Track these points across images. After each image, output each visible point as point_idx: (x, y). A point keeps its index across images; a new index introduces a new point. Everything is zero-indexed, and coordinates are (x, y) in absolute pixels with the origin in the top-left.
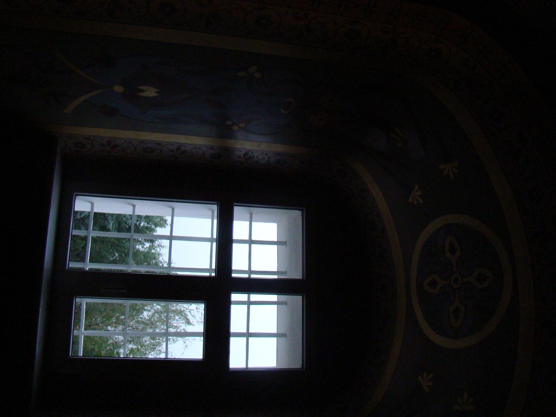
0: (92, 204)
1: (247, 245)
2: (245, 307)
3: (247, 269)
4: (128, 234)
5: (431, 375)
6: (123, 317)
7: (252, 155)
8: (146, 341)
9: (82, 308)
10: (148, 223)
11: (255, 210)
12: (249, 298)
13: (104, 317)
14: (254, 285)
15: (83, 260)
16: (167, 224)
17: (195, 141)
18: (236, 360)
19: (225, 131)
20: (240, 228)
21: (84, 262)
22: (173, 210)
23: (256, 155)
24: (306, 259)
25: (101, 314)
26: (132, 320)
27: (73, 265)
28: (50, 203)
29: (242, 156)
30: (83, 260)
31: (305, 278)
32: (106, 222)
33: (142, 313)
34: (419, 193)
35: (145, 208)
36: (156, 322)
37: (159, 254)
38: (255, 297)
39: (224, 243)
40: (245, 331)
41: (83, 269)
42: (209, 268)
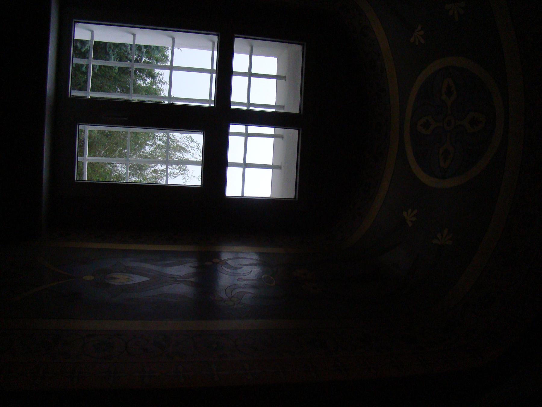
0: (92, 32)
1: (246, 78)
2: (243, 138)
3: (245, 101)
5: (415, 212)
6: (126, 151)
8: (148, 174)
9: (85, 141)
10: (149, 59)
11: (255, 43)
12: (247, 129)
13: (108, 150)
14: (251, 117)
15: (84, 88)
16: (168, 60)
18: (233, 188)
20: (240, 62)
21: (86, 90)
22: (173, 39)
24: (304, 97)
25: (105, 148)
26: (134, 154)
27: (75, 93)
28: (50, 30)
30: (84, 88)
31: (302, 112)
33: (144, 148)
35: (146, 37)
36: (158, 156)
37: (161, 90)
38: (252, 129)
39: (224, 74)
40: (241, 161)
41: (85, 97)
42: (208, 99)
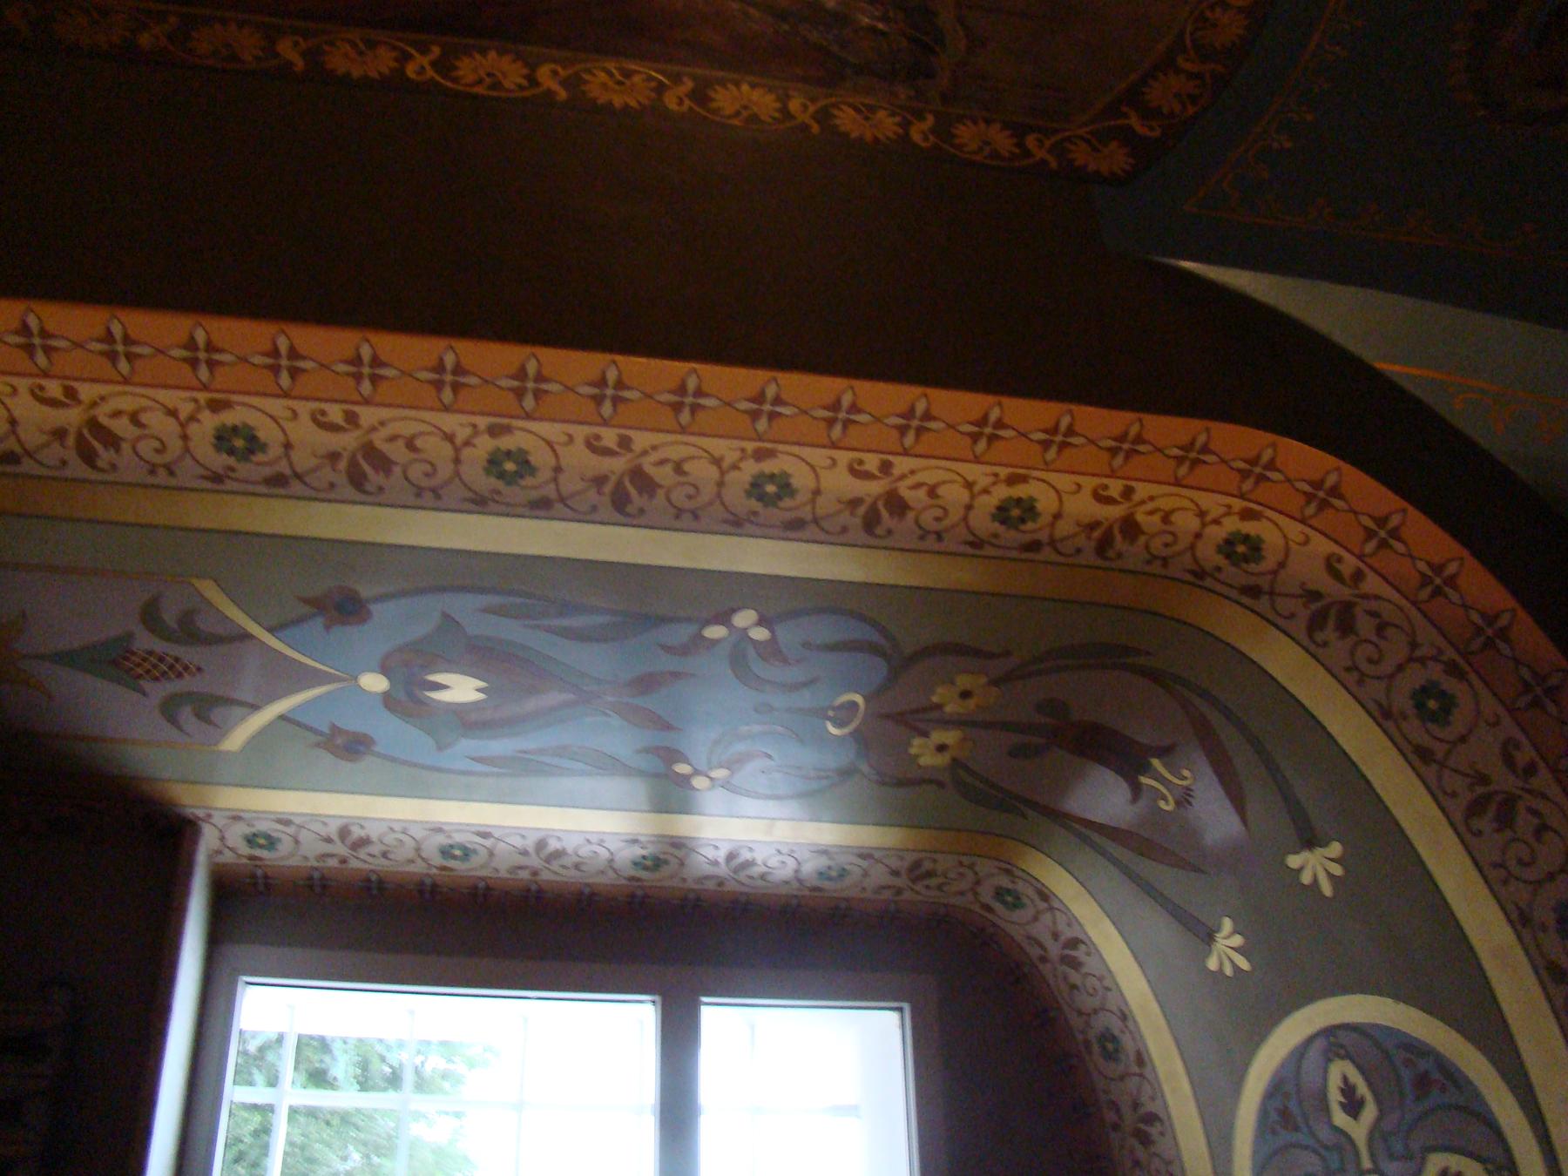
4: (391, 1094)
7: (362, 833)
17: (580, 822)
19: (670, 789)
23: (759, 856)
29: (721, 860)
32: (327, 1058)
34: (1237, 940)
